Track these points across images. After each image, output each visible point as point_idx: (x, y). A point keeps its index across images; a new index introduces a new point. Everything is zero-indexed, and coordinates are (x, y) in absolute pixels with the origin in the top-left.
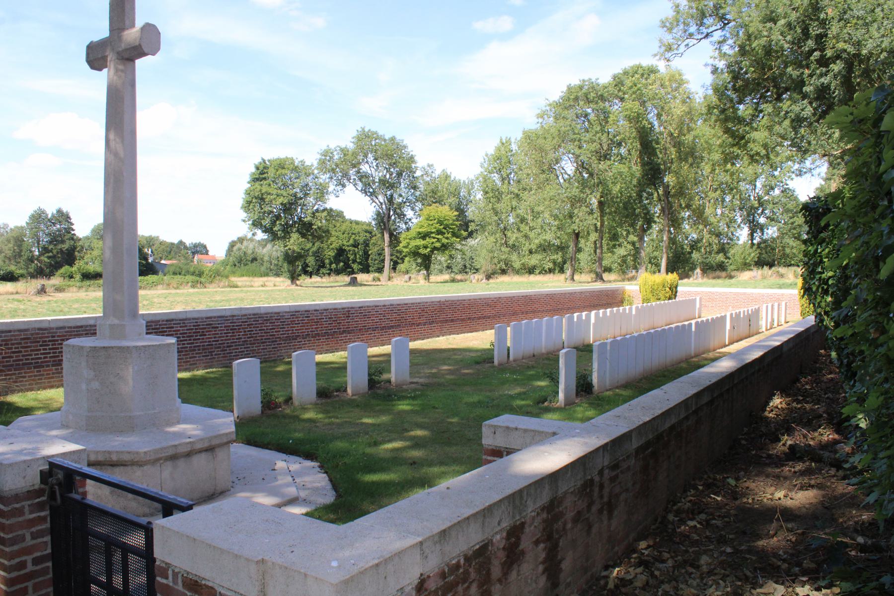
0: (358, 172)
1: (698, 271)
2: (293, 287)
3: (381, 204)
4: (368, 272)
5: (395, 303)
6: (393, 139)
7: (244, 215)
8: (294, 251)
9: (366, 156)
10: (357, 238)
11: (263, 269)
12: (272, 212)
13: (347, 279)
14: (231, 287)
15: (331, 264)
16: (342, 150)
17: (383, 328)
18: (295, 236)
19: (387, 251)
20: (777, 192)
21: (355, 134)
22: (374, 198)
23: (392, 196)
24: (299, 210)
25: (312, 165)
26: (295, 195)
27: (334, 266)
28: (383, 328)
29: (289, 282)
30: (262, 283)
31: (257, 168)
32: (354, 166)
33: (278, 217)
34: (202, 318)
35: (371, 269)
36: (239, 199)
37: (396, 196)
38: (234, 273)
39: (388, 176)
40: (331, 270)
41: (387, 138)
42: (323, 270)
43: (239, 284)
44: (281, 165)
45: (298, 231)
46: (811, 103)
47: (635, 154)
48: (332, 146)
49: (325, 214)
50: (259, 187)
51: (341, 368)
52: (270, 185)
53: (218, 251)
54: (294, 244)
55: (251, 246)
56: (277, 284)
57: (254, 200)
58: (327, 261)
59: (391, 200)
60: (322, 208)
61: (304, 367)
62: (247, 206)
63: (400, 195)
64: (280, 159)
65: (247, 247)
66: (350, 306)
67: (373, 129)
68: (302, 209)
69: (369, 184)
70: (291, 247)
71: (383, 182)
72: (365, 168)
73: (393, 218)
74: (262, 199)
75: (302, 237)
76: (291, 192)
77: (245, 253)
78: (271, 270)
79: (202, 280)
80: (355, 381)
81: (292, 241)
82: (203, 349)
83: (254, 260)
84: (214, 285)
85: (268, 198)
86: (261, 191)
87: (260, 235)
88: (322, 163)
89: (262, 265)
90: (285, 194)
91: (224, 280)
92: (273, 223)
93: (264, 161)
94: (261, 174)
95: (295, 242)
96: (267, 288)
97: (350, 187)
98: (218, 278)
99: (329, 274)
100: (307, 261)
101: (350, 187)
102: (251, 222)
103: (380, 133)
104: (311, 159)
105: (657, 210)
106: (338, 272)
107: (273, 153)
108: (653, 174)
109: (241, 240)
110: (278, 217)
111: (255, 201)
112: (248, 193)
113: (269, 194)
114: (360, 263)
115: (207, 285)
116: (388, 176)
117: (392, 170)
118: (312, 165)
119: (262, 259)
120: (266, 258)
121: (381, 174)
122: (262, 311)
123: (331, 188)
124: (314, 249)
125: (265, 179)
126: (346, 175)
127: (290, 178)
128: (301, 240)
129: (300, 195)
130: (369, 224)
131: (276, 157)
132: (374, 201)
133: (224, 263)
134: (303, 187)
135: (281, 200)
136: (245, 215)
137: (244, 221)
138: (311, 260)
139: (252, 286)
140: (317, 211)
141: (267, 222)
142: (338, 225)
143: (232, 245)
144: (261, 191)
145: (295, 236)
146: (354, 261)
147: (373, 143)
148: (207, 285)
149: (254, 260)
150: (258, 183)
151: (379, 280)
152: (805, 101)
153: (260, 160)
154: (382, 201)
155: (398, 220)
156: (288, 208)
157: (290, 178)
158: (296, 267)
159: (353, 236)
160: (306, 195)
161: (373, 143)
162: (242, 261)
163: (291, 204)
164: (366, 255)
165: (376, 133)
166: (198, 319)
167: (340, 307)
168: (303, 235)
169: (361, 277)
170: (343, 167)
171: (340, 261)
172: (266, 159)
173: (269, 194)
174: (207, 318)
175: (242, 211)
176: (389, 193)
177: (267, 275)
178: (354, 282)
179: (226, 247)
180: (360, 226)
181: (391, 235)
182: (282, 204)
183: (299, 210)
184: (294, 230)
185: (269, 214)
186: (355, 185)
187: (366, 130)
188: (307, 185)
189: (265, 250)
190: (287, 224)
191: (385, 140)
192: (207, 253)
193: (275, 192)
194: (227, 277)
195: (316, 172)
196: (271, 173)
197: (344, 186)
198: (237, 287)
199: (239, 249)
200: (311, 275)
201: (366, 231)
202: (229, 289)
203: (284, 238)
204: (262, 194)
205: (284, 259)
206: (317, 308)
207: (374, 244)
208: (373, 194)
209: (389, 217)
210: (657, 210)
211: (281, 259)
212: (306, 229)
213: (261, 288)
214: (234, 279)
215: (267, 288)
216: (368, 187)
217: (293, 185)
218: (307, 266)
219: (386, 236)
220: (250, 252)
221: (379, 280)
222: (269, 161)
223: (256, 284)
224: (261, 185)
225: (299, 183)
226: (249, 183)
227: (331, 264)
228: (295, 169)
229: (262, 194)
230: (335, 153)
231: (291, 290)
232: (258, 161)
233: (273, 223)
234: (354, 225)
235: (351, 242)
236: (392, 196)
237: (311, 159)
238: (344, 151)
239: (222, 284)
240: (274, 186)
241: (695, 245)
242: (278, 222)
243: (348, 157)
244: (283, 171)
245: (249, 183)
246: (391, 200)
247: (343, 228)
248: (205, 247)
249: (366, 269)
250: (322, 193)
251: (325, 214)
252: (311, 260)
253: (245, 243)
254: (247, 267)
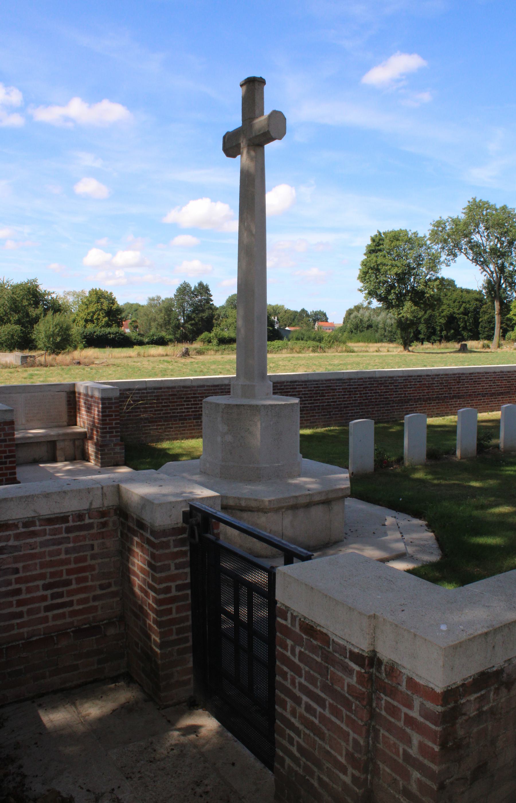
0: (470, 242)
2: (406, 353)
3: (492, 273)
4: (477, 339)
5: (505, 370)
6: (504, 208)
7: (360, 285)
8: (407, 319)
9: (477, 226)
10: (468, 306)
11: (377, 335)
12: (387, 282)
13: (458, 346)
14: (348, 352)
15: (441, 331)
16: (453, 221)
17: (492, 395)
18: (408, 304)
19: (497, 318)
21: (466, 204)
22: (485, 268)
23: (503, 264)
24: (412, 280)
25: (425, 237)
26: (408, 265)
27: (444, 333)
28: (492, 395)
29: (401, 348)
30: (376, 349)
31: (373, 240)
32: (466, 236)
33: (392, 287)
34: (322, 381)
35: (480, 336)
36: (356, 271)
37: (507, 264)
38: (350, 339)
39: (499, 245)
40: (441, 337)
41: (498, 207)
42: (434, 337)
43: (356, 349)
44: (396, 237)
45: (411, 299)
48: (445, 218)
49: (437, 283)
50: (375, 259)
51: (450, 432)
52: (385, 256)
53: (336, 318)
54: (407, 312)
55: (367, 314)
56: (391, 349)
57: (370, 271)
58: (438, 328)
59: (502, 269)
60: (434, 278)
61: (416, 428)
62: (364, 277)
63: (511, 264)
64: (396, 232)
65: (363, 315)
66: (461, 372)
67: (485, 199)
68: (414, 279)
69: (480, 254)
70: (405, 315)
71: (494, 251)
72: (476, 238)
73: (504, 286)
74: (378, 270)
75: (415, 305)
76: (405, 262)
77: (361, 321)
78: (385, 336)
79: (322, 345)
80: (464, 444)
81: (405, 309)
82: (323, 409)
83: (370, 326)
84: (332, 350)
85: (383, 269)
86: (376, 262)
87: (375, 304)
88: (434, 234)
89: (377, 331)
90: (399, 264)
91: (342, 345)
92: (388, 292)
93: (380, 234)
94: (377, 246)
95: (408, 309)
96: (382, 354)
97: (461, 258)
98: (336, 343)
99: (440, 341)
100: (419, 328)
101: (461, 258)
102: (366, 292)
103: (492, 203)
104: (423, 230)
106: (448, 339)
107: (389, 226)
109: (358, 308)
110: (392, 287)
111: (370, 272)
112: (364, 264)
113: (384, 265)
114: (470, 331)
115: (326, 350)
116: (499, 245)
117: (503, 239)
118: (425, 237)
119: (377, 326)
120: (381, 326)
121: (492, 243)
122: (378, 375)
123: (443, 257)
124: (426, 316)
125: (380, 250)
126: (457, 245)
127: (404, 250)
128: (414, 308)
129: (414, 265)
130: (480, 292)
131: (390, 230)
132: (485, 270)
133: (342, 330)
134: (416, 257)
135: (395, 270)
136: (362, 284)
137: (360, 290)
138: (422, 327)
139: (367, 351)
140: (429, 280)
141: (382, 291)
142: (449, 294)
143: (350, 312)
144: (376, 262)
145: (408, 304)
146: (465, 328)
147: (485, 213)
148: (326, 350)
149: (370, 326)
150: (373, 255)
151: (488, 347)
153: (376, 233)
154: (492, 269)
155: (509, 289)
156: (402, 278)
157: (404, 250)
158: (409, 334)
159: (464, 305)
160: (419, 265)
161: (485, 213)
162: (358, 327)
163: (405, 274)
164: (476, 323)
165: (487, 203)
166: (318, 381)
167: (451, 373)
168: (416, 304)
169: (471, 344)
170: (454, 237)
171: (450, 329)
172: (382, 232)
173: (384, 265)
174: (326, 380)
175: (358, 281)
176: (500, 262)
177: (381, 341)
178: (464, 349)
179: (343, 314)
180: (471, 295)
181: (502, 304)
182: (396, 274)
183: (412, 280)
184: (408, 298)
185: (384, 284)
186: (466, 254)
187: (478, 200)
188: (420, 255)
189: (379, 318)
190: (400, 293)
191: (496, 210)
192: (326, 320)
193: (390, 263)
194: (344, 343)
195: (428, 242)
196: (386, 245)
197: (455, 255)
198: (353, 352)
199: (356, 317)
200: (422, 341)
201: (477, 300)
202: (346, 354)
203: (398, 306)
204: (378, 265)
205: (398, 326)
206: (429, 373)
207: (485, 312)
208: (484, 264)
209: (500, 286)
211: (394, 326)
212: (418, 297)
213: (375, 354)
214: (351, 345)
215: (382, 354)
216: (479, 256)
217: (406, 256)
218: (419, 333)
219: (497, 305)
220: (366, 319)
221: (488, 347)
222: (384, 233)
223: (371, 349)
224: (377, 257)
225: (413, 254)
226: (365, 254)
227: (441, 331)
228: (409, 241)
229: (378, 265)
230: (447, 224)
231: (404, 355)
232: (374, 233)
233: (388, 292)
234: (464, 294)
235: (462, 309)
236: (503, 264)
237: (423, 230)
238: (456, 222)
239: (340, 349)
240: (388, 257)
242: (392, 291)
243: (460, 227)
244: (398, 243)
245: (365, 254)
246: (502, 269)
247: (454, 296)
248: (325, 315)
249: (476, 337)
250: (434, 263)
251: (437, 283)
252: (422, 327)
253: (361, 311)
254: (363, 334)
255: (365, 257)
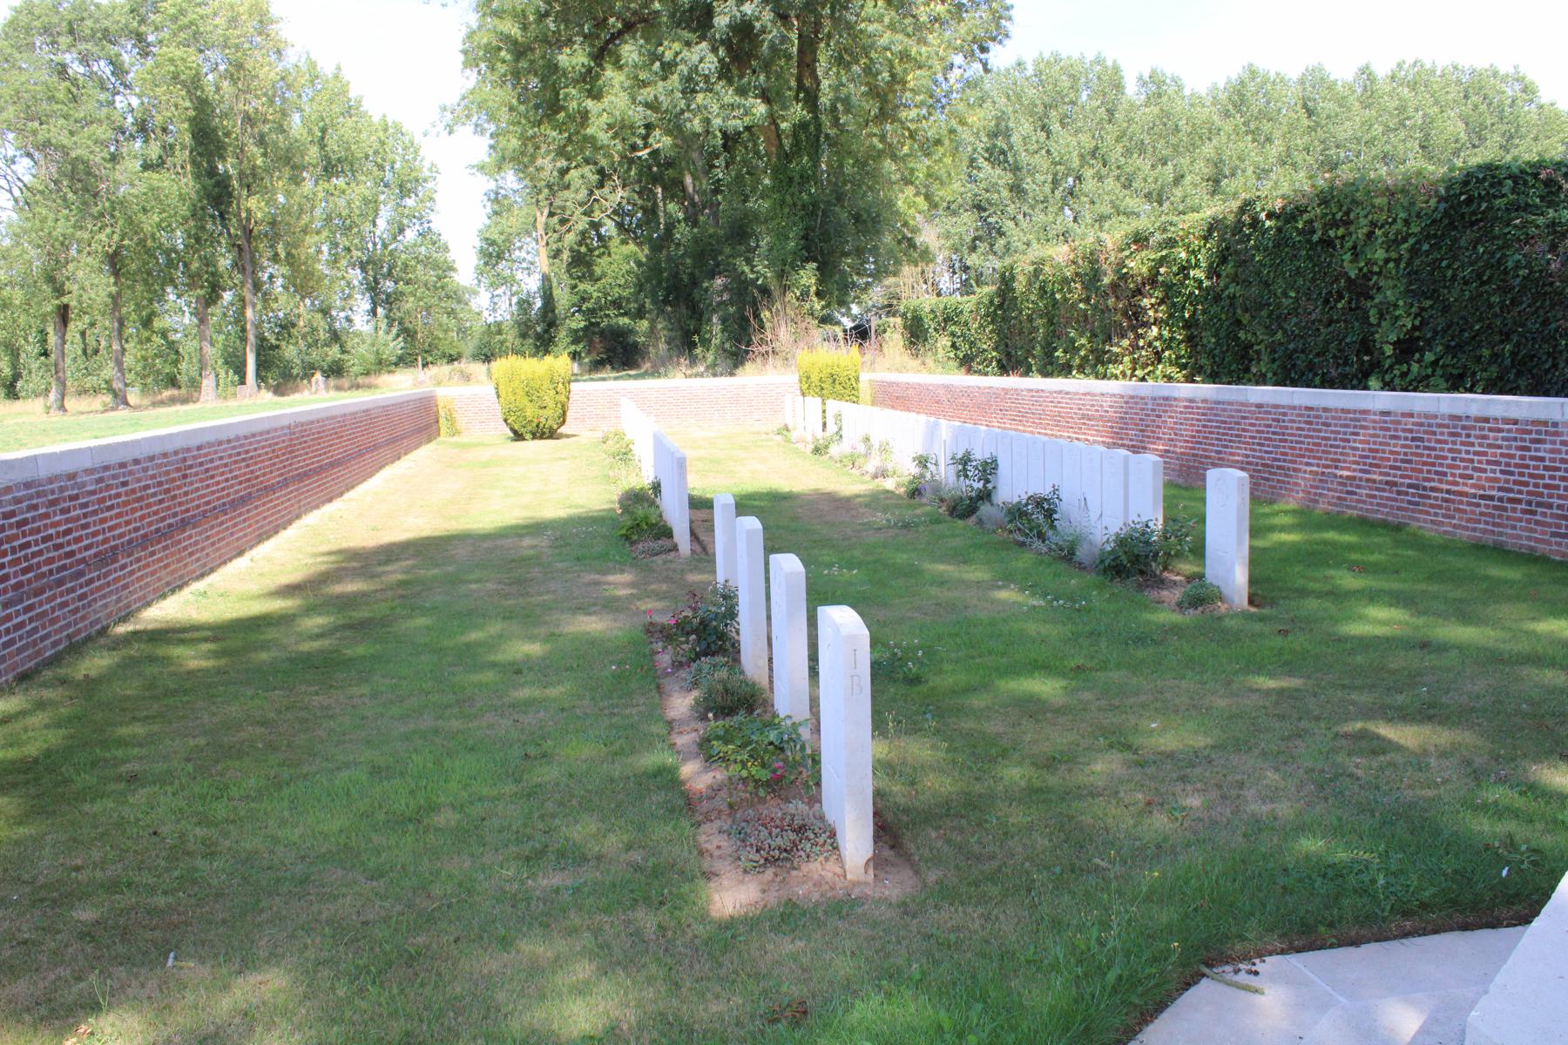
1: (318, 376)
20: (410, 235)
46: (714, 50)
47: (182, 156)
105: (225, 262)
108: (217, 196)
122: (43, 473)
152: (704, 44)
210: (225, 262)
241: (286, 327)
255: (376, 119)
